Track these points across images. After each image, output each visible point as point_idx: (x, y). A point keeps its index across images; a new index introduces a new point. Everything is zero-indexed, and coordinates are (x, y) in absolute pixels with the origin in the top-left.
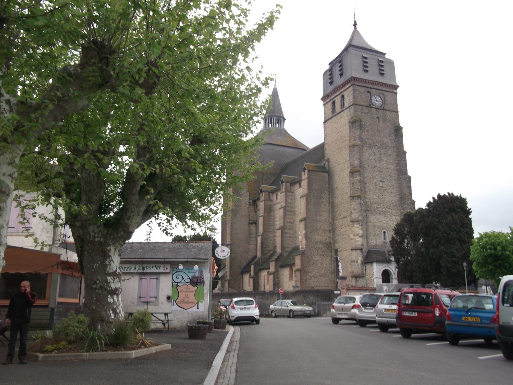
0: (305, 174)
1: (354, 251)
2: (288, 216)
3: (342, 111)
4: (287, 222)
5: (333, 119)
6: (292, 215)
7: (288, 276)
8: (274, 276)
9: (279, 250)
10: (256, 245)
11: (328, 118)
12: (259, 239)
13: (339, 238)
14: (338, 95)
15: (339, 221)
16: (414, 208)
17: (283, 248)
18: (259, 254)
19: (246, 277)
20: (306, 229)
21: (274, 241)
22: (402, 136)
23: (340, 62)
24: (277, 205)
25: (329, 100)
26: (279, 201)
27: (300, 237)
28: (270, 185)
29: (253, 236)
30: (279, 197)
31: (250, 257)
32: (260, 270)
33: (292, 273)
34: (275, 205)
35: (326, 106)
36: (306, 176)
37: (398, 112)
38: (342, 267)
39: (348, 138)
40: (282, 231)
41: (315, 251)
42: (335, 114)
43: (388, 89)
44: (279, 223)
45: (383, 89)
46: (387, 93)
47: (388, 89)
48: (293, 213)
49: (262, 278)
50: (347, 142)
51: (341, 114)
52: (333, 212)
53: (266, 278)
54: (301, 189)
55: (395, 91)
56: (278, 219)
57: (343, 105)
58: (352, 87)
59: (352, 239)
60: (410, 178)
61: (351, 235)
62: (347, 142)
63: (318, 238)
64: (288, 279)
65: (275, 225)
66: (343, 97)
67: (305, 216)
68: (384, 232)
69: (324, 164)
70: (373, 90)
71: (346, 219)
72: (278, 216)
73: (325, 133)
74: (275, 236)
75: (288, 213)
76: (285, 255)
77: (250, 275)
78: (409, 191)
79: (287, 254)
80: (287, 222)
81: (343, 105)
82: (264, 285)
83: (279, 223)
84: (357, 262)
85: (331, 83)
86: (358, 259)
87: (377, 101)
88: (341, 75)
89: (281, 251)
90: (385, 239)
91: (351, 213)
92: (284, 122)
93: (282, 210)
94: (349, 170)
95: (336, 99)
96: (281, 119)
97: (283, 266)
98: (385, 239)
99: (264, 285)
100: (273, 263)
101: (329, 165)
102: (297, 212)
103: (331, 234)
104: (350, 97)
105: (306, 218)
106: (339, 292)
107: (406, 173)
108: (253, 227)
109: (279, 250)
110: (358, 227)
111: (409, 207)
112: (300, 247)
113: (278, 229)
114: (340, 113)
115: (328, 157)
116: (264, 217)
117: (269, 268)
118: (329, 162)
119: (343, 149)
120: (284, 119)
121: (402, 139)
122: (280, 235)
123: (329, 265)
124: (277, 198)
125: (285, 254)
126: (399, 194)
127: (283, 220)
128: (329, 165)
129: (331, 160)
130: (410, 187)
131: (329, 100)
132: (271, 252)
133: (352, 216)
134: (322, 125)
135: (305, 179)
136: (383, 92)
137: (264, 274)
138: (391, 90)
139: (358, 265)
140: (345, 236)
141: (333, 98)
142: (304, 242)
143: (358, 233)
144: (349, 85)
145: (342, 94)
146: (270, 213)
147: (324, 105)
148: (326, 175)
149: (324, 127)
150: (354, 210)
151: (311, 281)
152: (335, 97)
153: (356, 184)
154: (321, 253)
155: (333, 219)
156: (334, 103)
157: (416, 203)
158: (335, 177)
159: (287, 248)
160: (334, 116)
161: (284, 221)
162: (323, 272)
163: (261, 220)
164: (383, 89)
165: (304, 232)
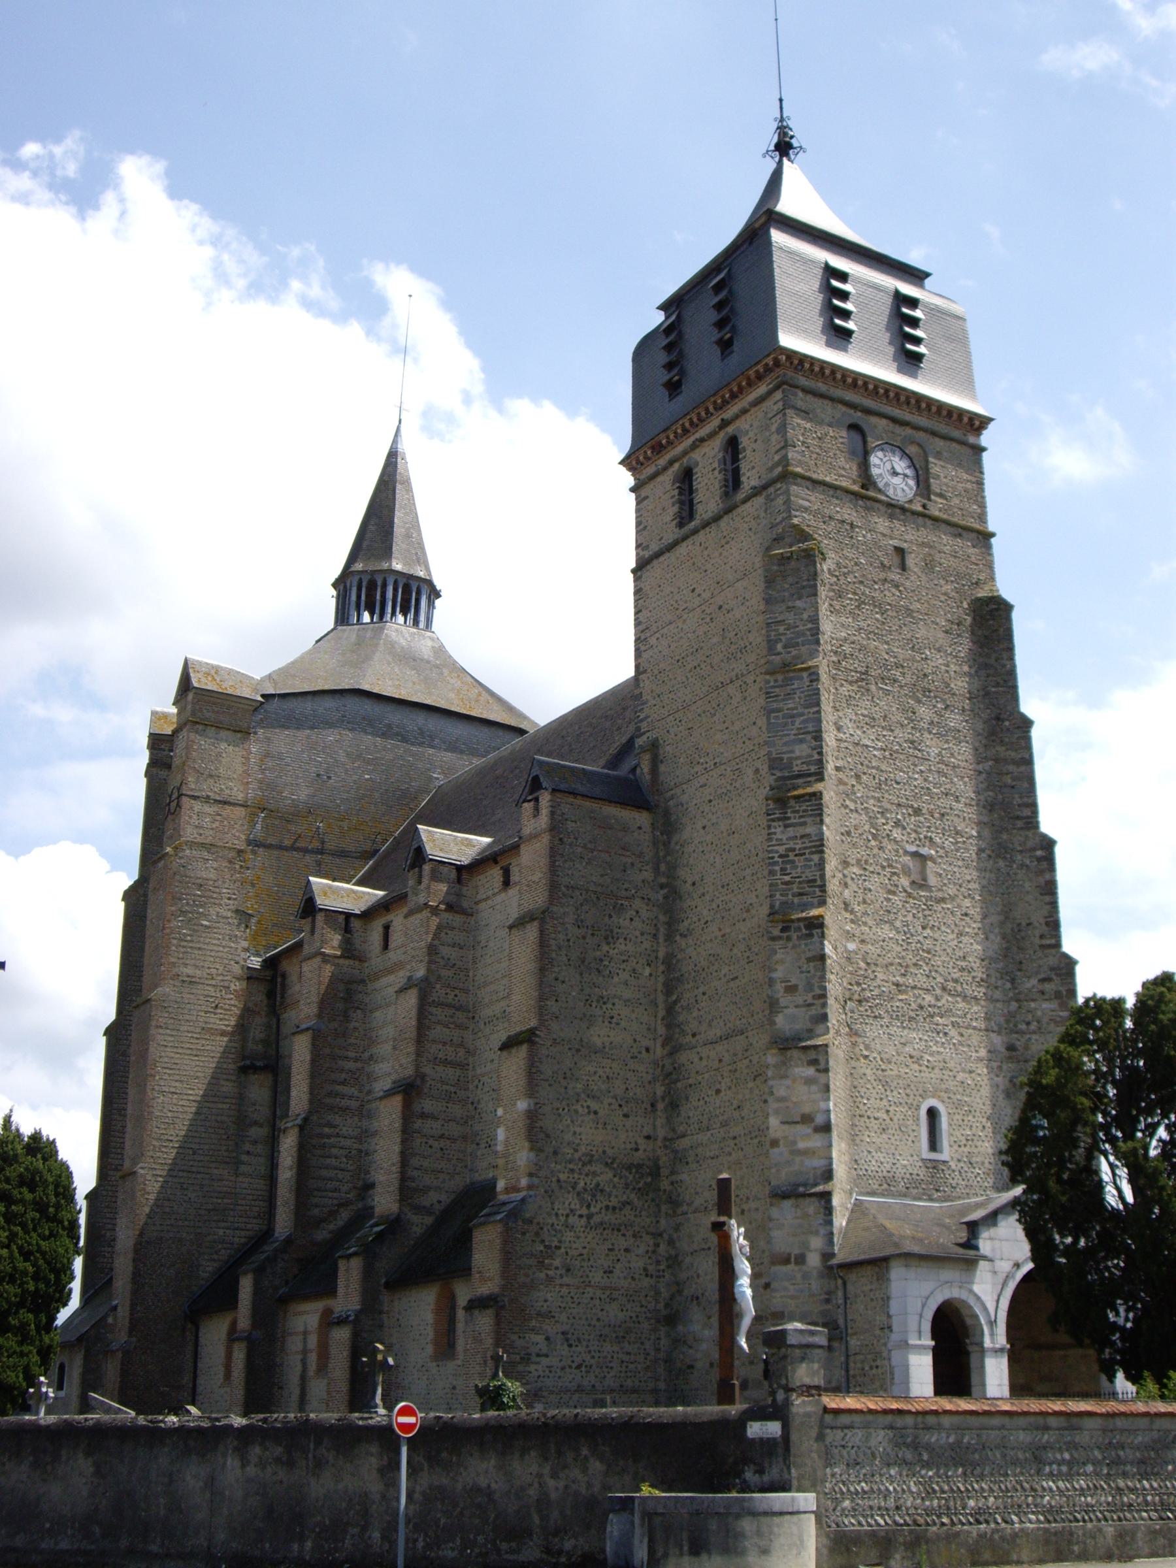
0: (537, 811)
1: (787, 1204)
2: (437, 1032)
3: (728, 511)
4: (436, 1061)
5: (682, 549)
6: (459, 1026)
7: (430, 1333)
8: (356, 1335)
9: (385, 1202)
10: (273, 1165)
11: (655, 547)
12: (288, 1144)
13: (703, 1137)
14: (712, 435)
15: (705, 1051)
16: (1072, 993)
17: (406, 1190)
18: (284, 1222)
19: (214, 1334)
20: (532, 1088)
21: (362, 1157)
22: (1010, 649)
23: (718, 288)
24: (384, 981)
25: (662, 462)
26: (393, 956)
27: (501, 1134)
28: (358, 883)
29: (255, 1132)
30: (396, 939)
31: (239, 1238)
32: (285, 1301)
33: (452, 1320)
34: (376, 976)
35: (644, 492)
36: (544, 819)
37: (985, 537)
38: (755, 1277)
39: (757, 638)
40: (407, 1105)
41: (576, 1204)
42: (741, 495)
43: (942, 428)
44: (391, 1063)
45: (922, 421)
46: (939, 443)
47: (942, 428)
48: (465, 1012)
49: (294, 1345)
50: (751, 658)
51: (723, 523)
52: (670, 1010)
53: (313, 1341)
54: (512, 892)
55: (971, 439)
56: (385, 1049)
57: (733, 480)
58: (778, 395)
59: (775, 1143)
60: (1048, 845)
61: (774, 1122)
62: (751, 658)
63: (585, 1134)
64: (430, 1349)
65: (371, 1078)
66: (733, 446)
67: (533, 1023)
68: (932, 1113)
69: (633, 770)
70: (874, 420)
71: (739, 1042)
72: (389, 1032)
73: (637, 623)
74: (365, 1135)
75: (438, 1013)
76: (417, 1230)
77: (234, 1323)
78: (1046, 910)
79: (429, 1220)
80: (436, 1061)
81: (733, 480)
82: (303, 1378)
83: (391, 1063)
84: (801, 1259)
85: (673, 388)
86: (805, 1246)
87: (892, 473)
88: (726, 346)
89: (394, 1208)
90: (934, 1145)
91: (773, 1006)
92: (431, 605)
93: (411, 1000)
94: (764, 791)
95: (696, 455)
96: (414, 595)
97: (405, 1279)
98: (934, 1145)
99: (303, 1378)
100: (356, 1264)
101: (654, 770)
102: (487, 1012)
103: (660, 1122)
104: (767, 441)
105: (532, 1032)
106: (773, 1428)
107: (1032, 821)
108: (258, 1091)
109: (385, 1202)
110: (809, 1081)
111: (1047, 987)
112: (501, 1185)
113: (389, 1094)
114: (717, 519)
115: (651, 735)
116: (317, 1037)
117: (332, 1292)
118: (655, 761)
119: (731, 689)
120: (435, 594)
121: (1011, 658)
122: (398, 1125)
123: (646, 1282)
124: (386, 946)
125: (419, 1224)
126: (1002, 924)
127: (411, 1049)
128: (654, 770)
129: (667, 750)
130: (1050, 889)
131: (662, 462)
132: (345, 1215)
133: (780, 1020)
134: (628, 584)
135: (535, 836)
136: (920, 436)
137: (306, 1318)
138: (956, 434)
139: (806, 1276)
140: (736, 1130)
141: (685, 453)
142: (523, 1157)
143: (807, 1109)
144: (762, 389)
145: (730, 430)
146: (347, 1018)
147: (632, 490)
148: (642, 818)
149: (638, 592)
150: (791, 989)
151: (553, 1361)
152: (694, 447)
153: (799, 862)
154: (608, 1217)
155: (674, 1047)
156: (687, 476)
157: (1079, 970)
158: (686, 834)
159: (426, 1189)
160: (685, 538)
161: (418, 1054)
162: (614, 1313)
163: (300, 1052)
164: (922, 421)
165: (522, 1105)
